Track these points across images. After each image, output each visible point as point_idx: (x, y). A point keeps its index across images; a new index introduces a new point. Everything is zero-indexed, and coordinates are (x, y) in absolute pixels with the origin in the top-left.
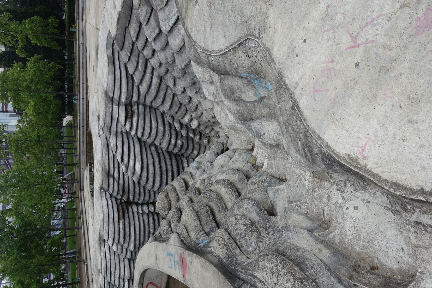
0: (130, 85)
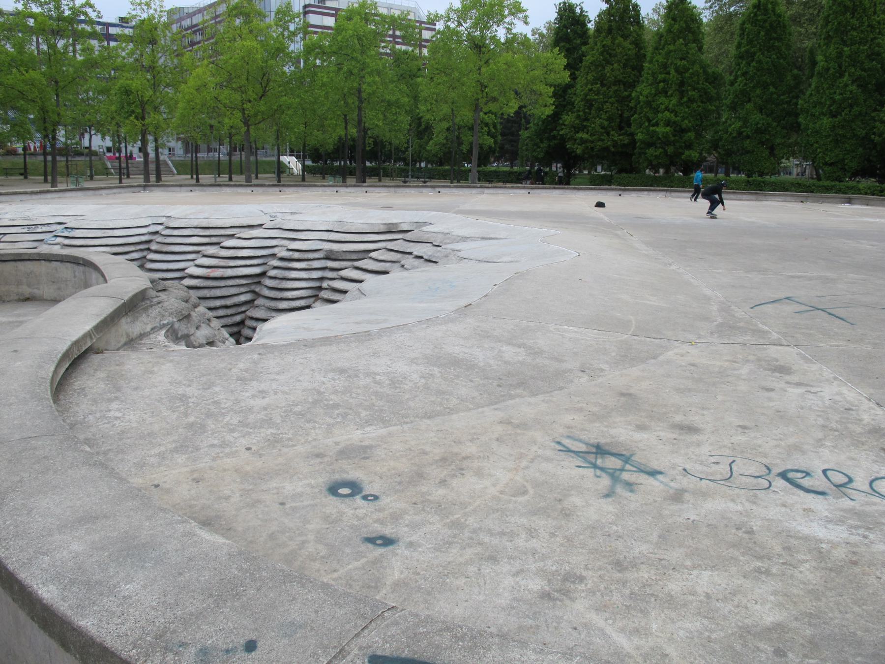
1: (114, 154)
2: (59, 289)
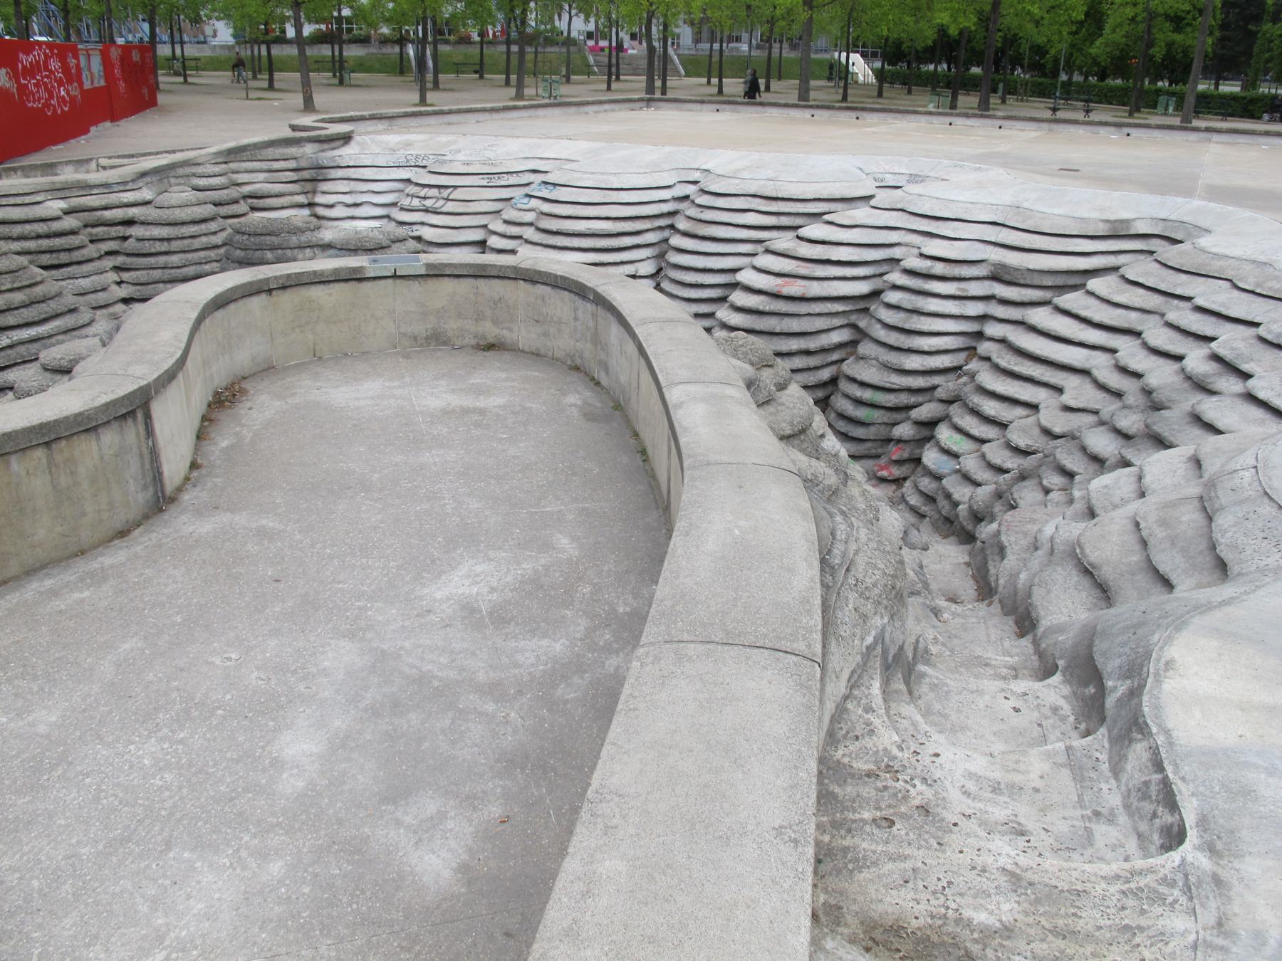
0: (1049, 281)
2: (546, 334)
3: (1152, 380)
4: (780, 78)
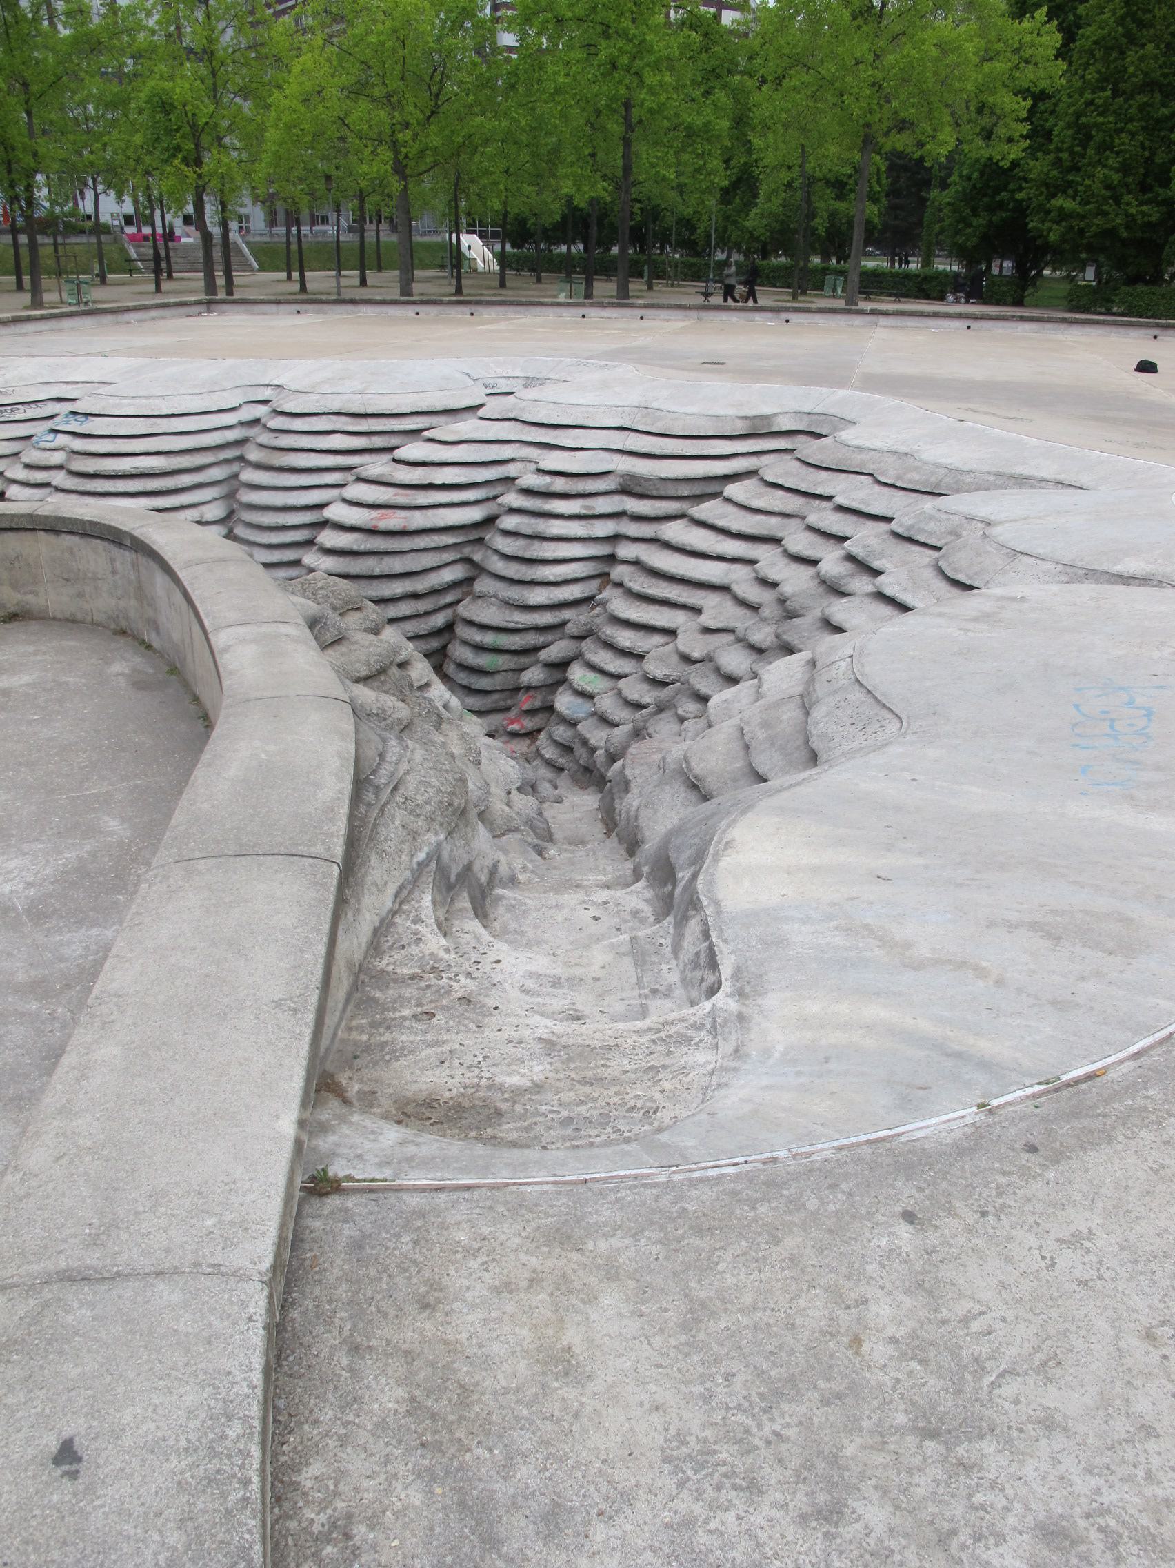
0: (685, 490)
1: (139, 230)
2: (80, 595)
3: (787, 589)
4: (380, 269)
